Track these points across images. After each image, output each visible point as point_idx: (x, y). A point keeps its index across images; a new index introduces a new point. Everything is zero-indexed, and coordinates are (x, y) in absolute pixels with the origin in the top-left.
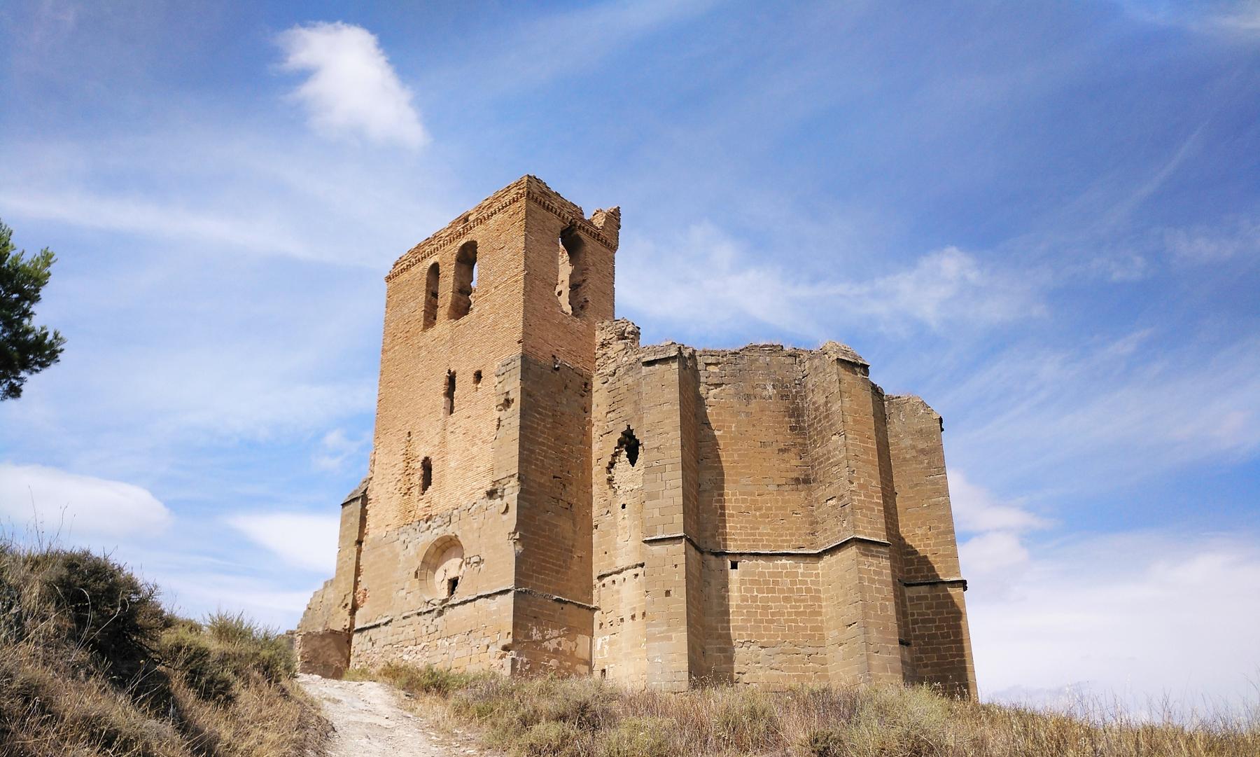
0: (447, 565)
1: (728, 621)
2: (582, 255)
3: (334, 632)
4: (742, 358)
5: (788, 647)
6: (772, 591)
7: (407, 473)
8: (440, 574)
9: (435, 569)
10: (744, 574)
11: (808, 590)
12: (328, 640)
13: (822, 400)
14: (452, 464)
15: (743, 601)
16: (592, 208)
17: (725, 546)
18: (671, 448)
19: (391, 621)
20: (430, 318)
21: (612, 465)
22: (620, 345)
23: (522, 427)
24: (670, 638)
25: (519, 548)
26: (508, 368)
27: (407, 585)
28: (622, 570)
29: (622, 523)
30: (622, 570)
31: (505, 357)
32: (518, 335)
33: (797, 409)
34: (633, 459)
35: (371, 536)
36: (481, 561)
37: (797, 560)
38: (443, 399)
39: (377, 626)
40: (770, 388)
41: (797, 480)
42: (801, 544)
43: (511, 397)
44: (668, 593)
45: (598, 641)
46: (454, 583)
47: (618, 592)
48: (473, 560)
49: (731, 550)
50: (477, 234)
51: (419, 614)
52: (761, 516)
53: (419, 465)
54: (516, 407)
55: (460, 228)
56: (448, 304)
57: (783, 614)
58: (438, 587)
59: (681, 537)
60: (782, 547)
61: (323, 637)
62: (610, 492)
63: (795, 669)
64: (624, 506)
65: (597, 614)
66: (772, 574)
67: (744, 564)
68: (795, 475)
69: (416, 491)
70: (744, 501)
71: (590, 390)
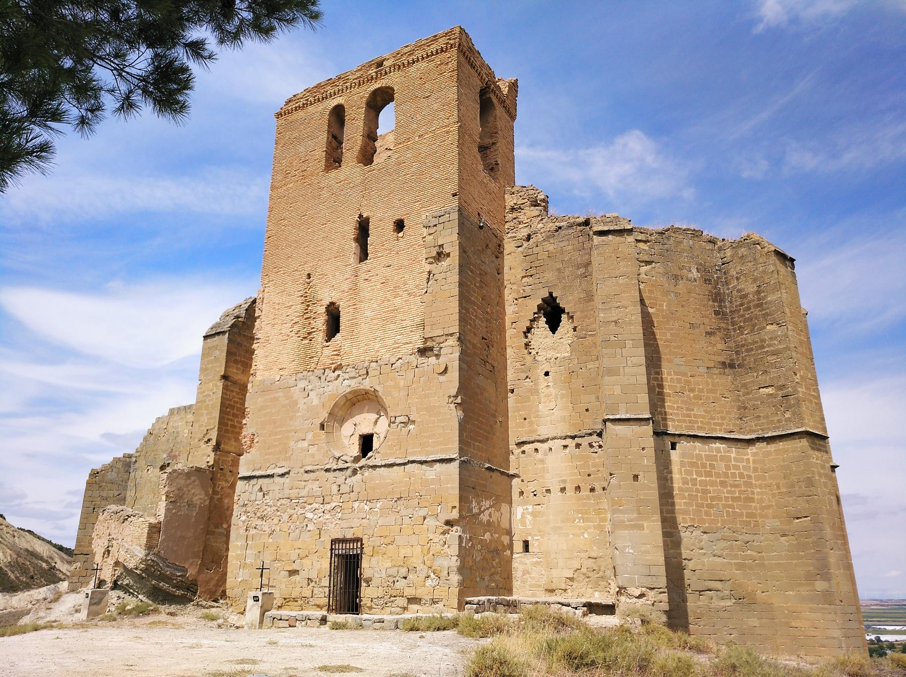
0: (357, 419)
1: (673, 504)
2: (491, 119)
3: (199, 470)
4: (668, 238)
5: (728, 534)
6: (708, 474)
7: (307, 314)
8: (347, 428)
9: (342, 421)
10: (683, 455)
11: (741, 475)
12: (193, 478)
13: (751, 288)
14: (368, 313)
15: (684, 483)
16: (503, 76)
17: (666, 426)
18: (630, 323)
19: (288, 473)
20: (334, 159)
21: (529, 330)
22: (535, 211)
23: (461, 284)
24: (641, 527)
25: (460, 413)
26: (442, 220)
27: (310, 436)
28: (547, 440)
29: (546, 391)
30: (547, 440)
31: (436, 209)
32: (453, 187)
33: (718, 294)
34: (554, 325)
35: (259, 377)
36: (410, 421)
37: (730, 444)
38: (354, 244)
39: (272, 476)
40: (694, 271)
41: (724, 363)
42: (731, 428)
43: (446, 250)
44: (636, 477)
45: (518, 511)
46: (366, 443)
47: (542, 461)
48: (399, 420)
49: (671, 430)
50: (392, 80)
51: (327, 470)
52: (695, 397)
53: (322, 310)
54: (453, 261)
55: (372, 72)
56: (358, 148)
57: (720, 499)
58: (346, 441)
59: (648, 419)
60: (715, 430)
61: (188, 475)
62: (529, 359)
63: (735, 557)
64: (547, 374)
65: (515, 481)
66: (708, 457)
67: (682, 445)
68: (722, 359)
69: (320, 337)
70: (679, 381)
71: (502, 253)
